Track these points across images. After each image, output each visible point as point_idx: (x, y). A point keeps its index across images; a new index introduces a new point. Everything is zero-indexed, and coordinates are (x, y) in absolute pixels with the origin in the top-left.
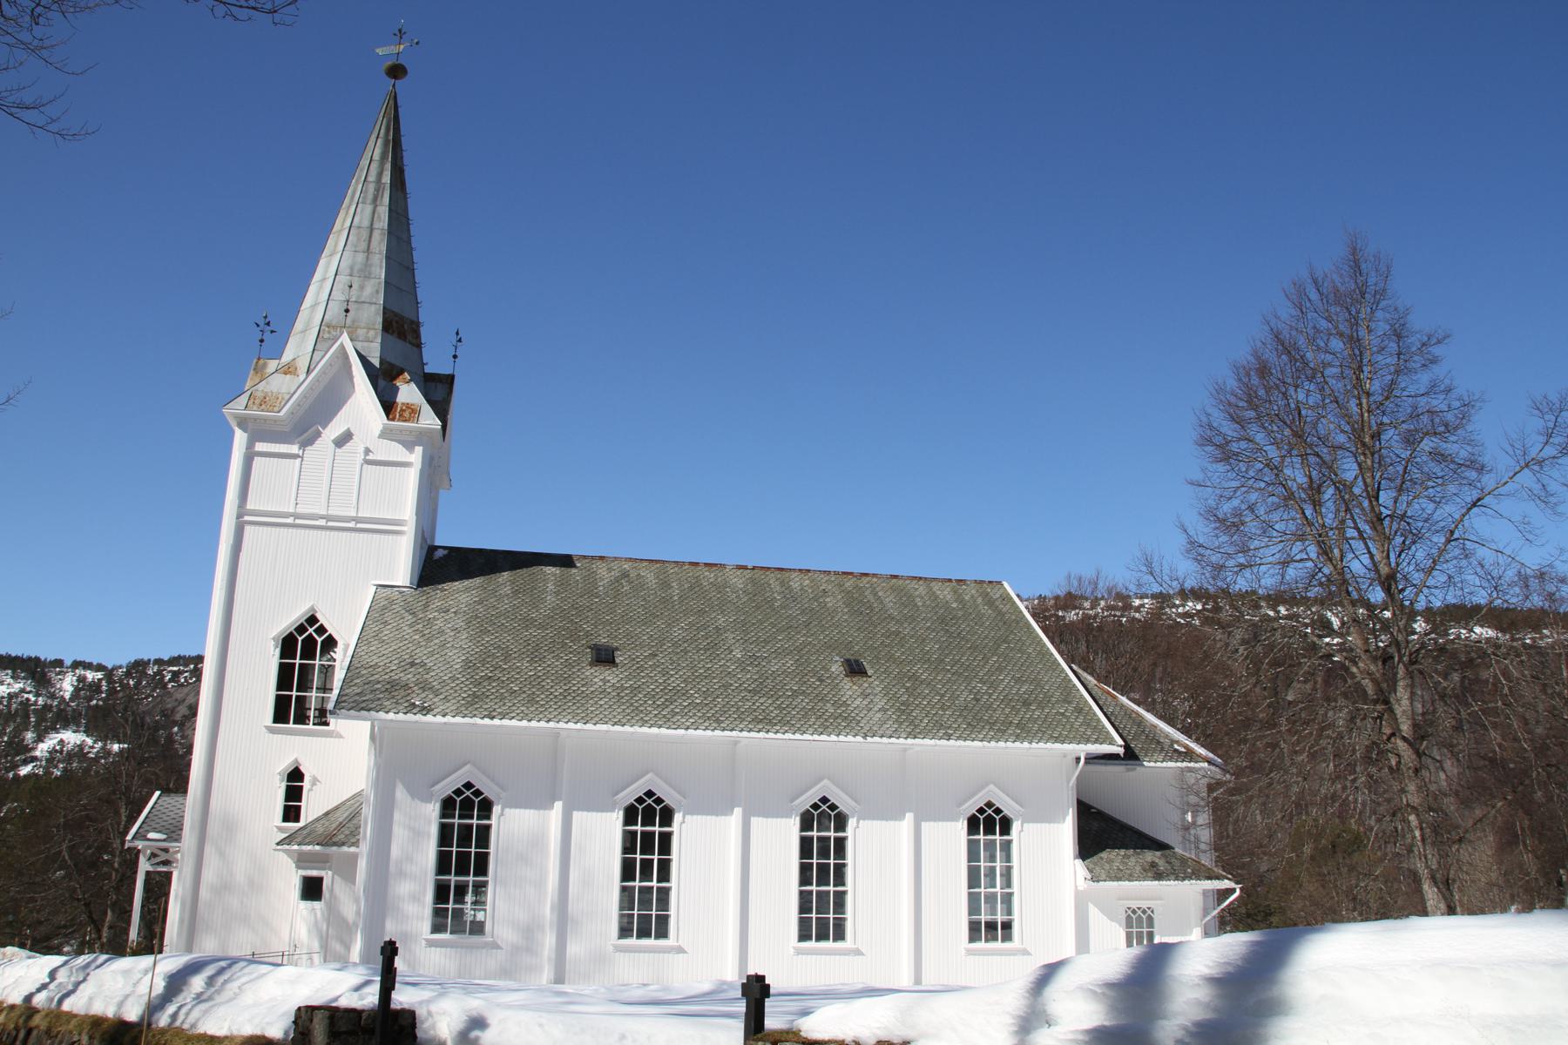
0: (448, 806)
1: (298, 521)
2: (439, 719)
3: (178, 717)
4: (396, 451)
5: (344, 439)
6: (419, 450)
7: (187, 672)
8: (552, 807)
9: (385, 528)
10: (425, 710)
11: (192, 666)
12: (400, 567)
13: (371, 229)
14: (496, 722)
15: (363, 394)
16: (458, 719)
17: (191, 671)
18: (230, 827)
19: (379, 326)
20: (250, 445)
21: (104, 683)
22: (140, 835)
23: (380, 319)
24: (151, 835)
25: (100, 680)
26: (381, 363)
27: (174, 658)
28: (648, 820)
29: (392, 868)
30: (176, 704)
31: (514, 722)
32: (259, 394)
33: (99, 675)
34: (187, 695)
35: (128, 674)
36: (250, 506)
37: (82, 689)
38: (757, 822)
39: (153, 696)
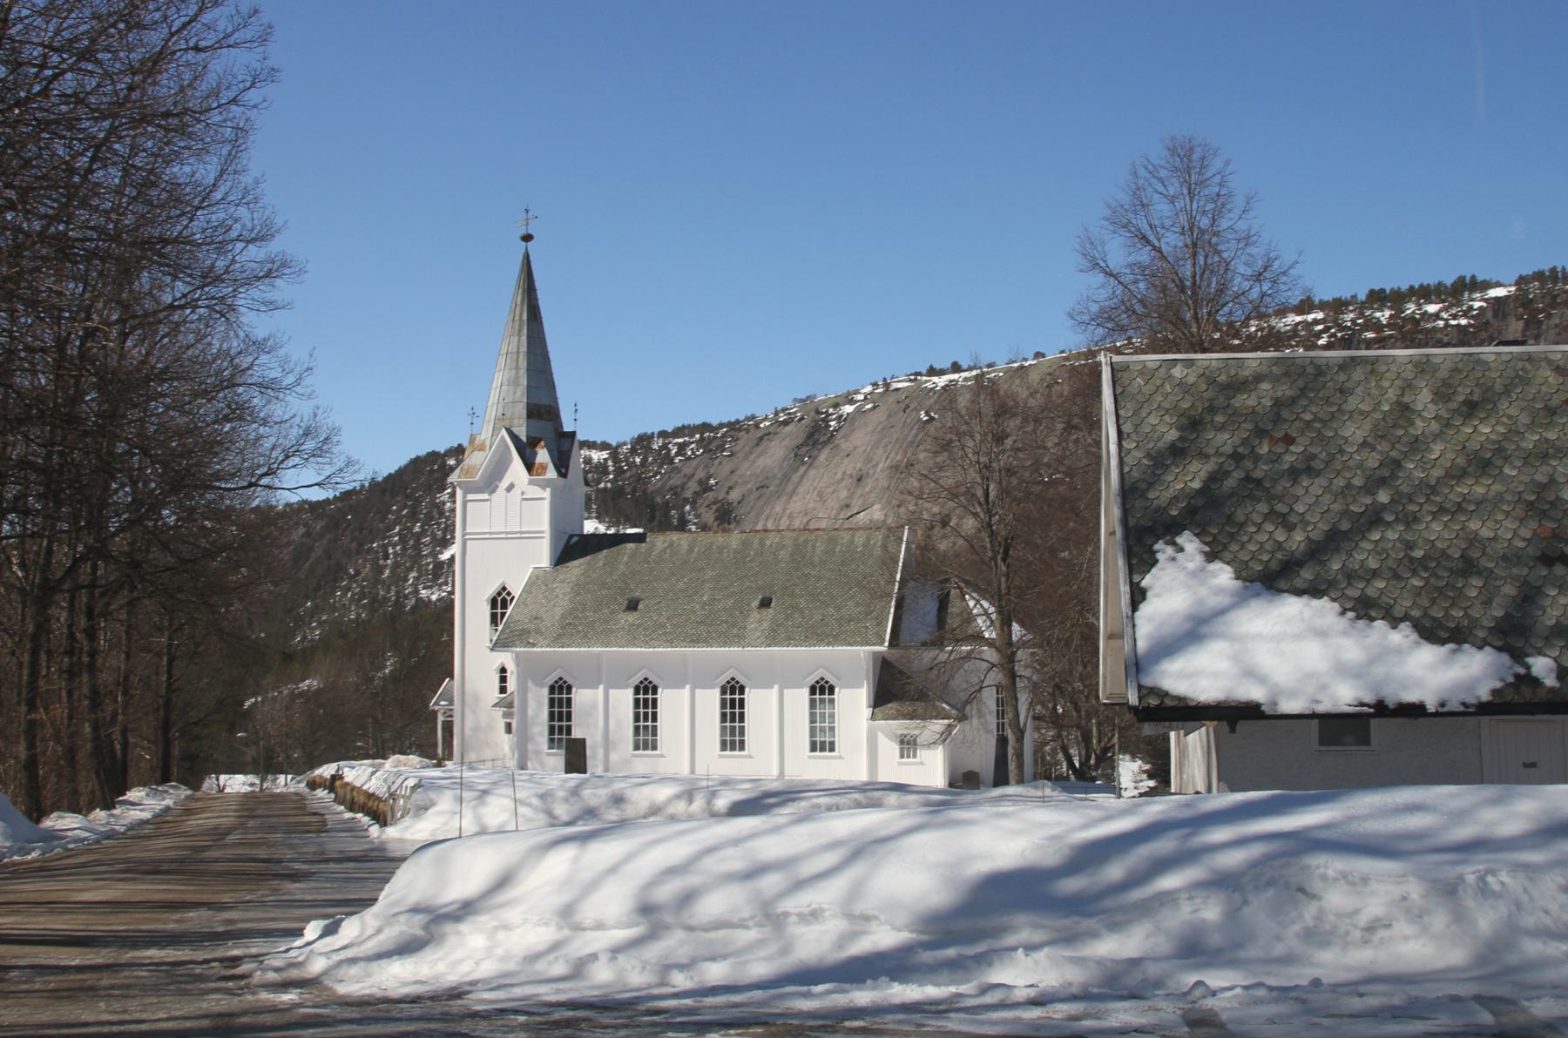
0: (552, 689)
1: (492, 537)
2: (539, 649)
3: (688, 494)
4: (536, 492)
5: (510, 488)
6: (548, 490)
7: (693, 443)
8: (598, 688)
9: (535, 536)
10: (534, 645)
11: (698, 436)
12: (543, 558)
13: (518, 353)
14: (565, 649)
15: (517, 464)
16: (547, 649)
17: (697, 442)
18: (476, 699)
19: (525, 416)
20: (464, 497)
21: (610, 463)
22: (436, 703)
23: (525, 412)
24: (442, 703)
25: (605, 460)
26: (528, 437)
27: (678, 428)
28: (646, 692)
29: (529, 720)
30: (686, 480)
31: (573, 649)
32: (465, 467)
33: (604, 455)
34: (696, 468)
35: (633, 451)
36: (468, 531)
37: (590, 472)
38: (698, 692)
39: (660, 473)
